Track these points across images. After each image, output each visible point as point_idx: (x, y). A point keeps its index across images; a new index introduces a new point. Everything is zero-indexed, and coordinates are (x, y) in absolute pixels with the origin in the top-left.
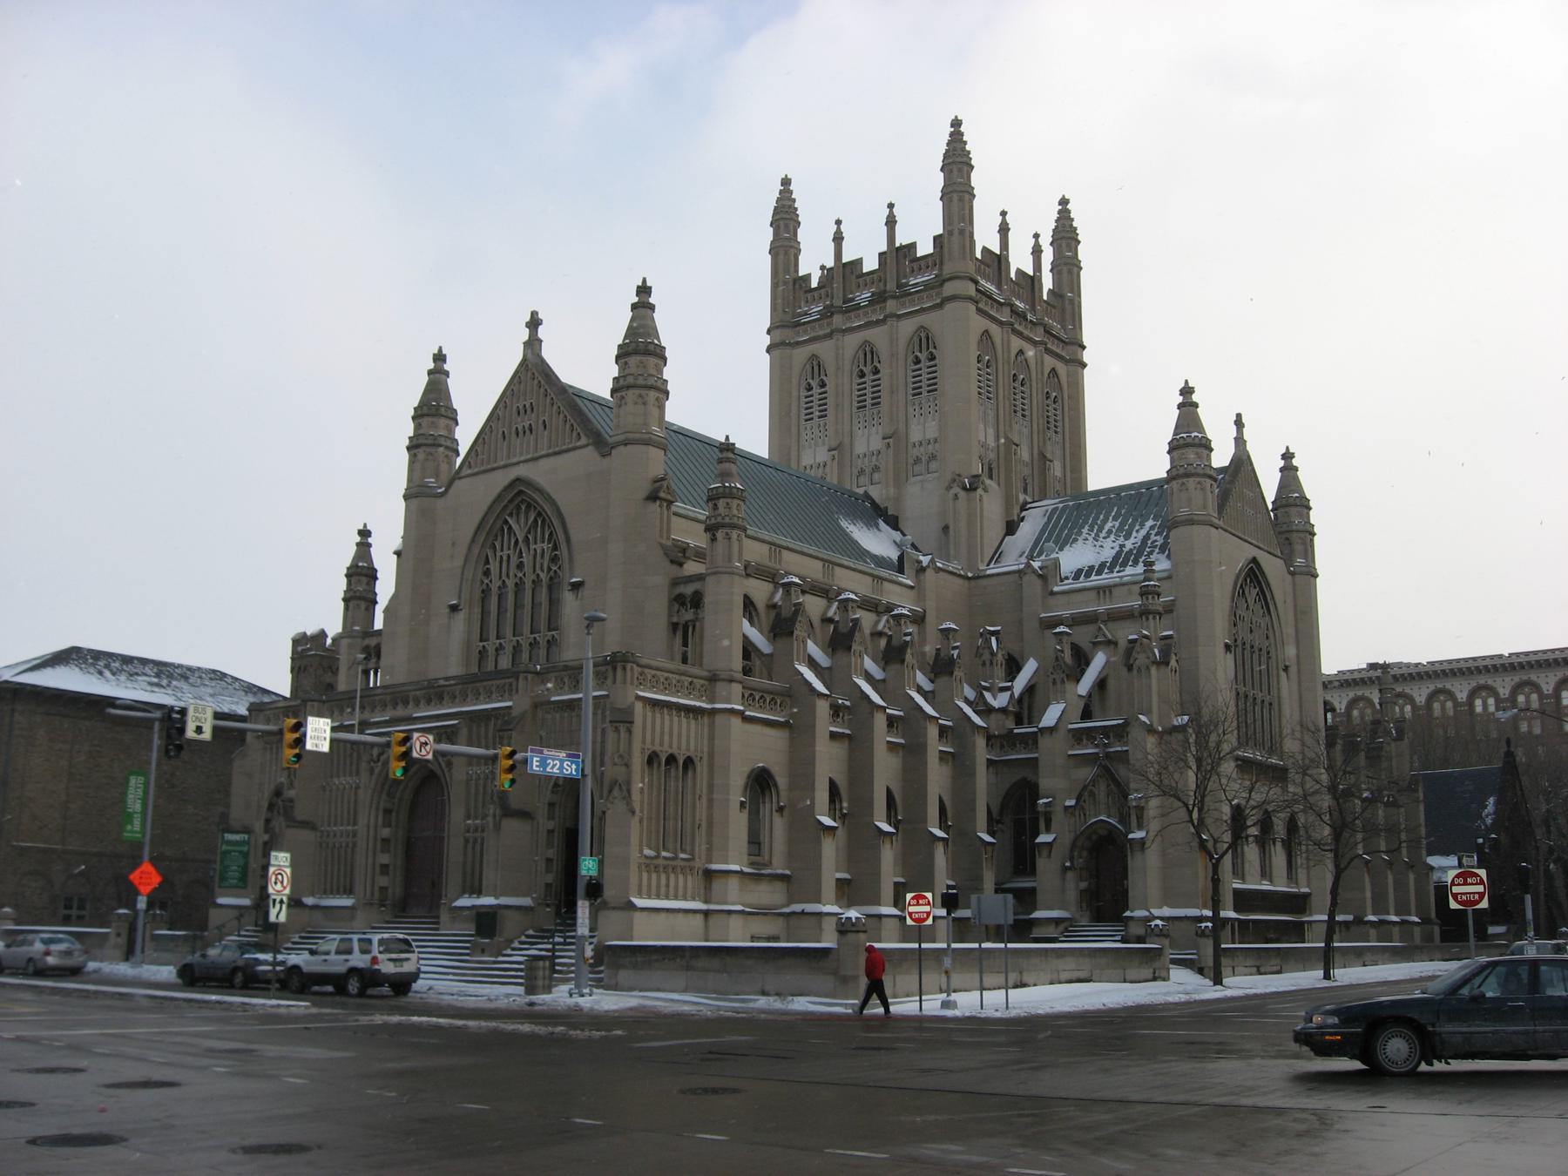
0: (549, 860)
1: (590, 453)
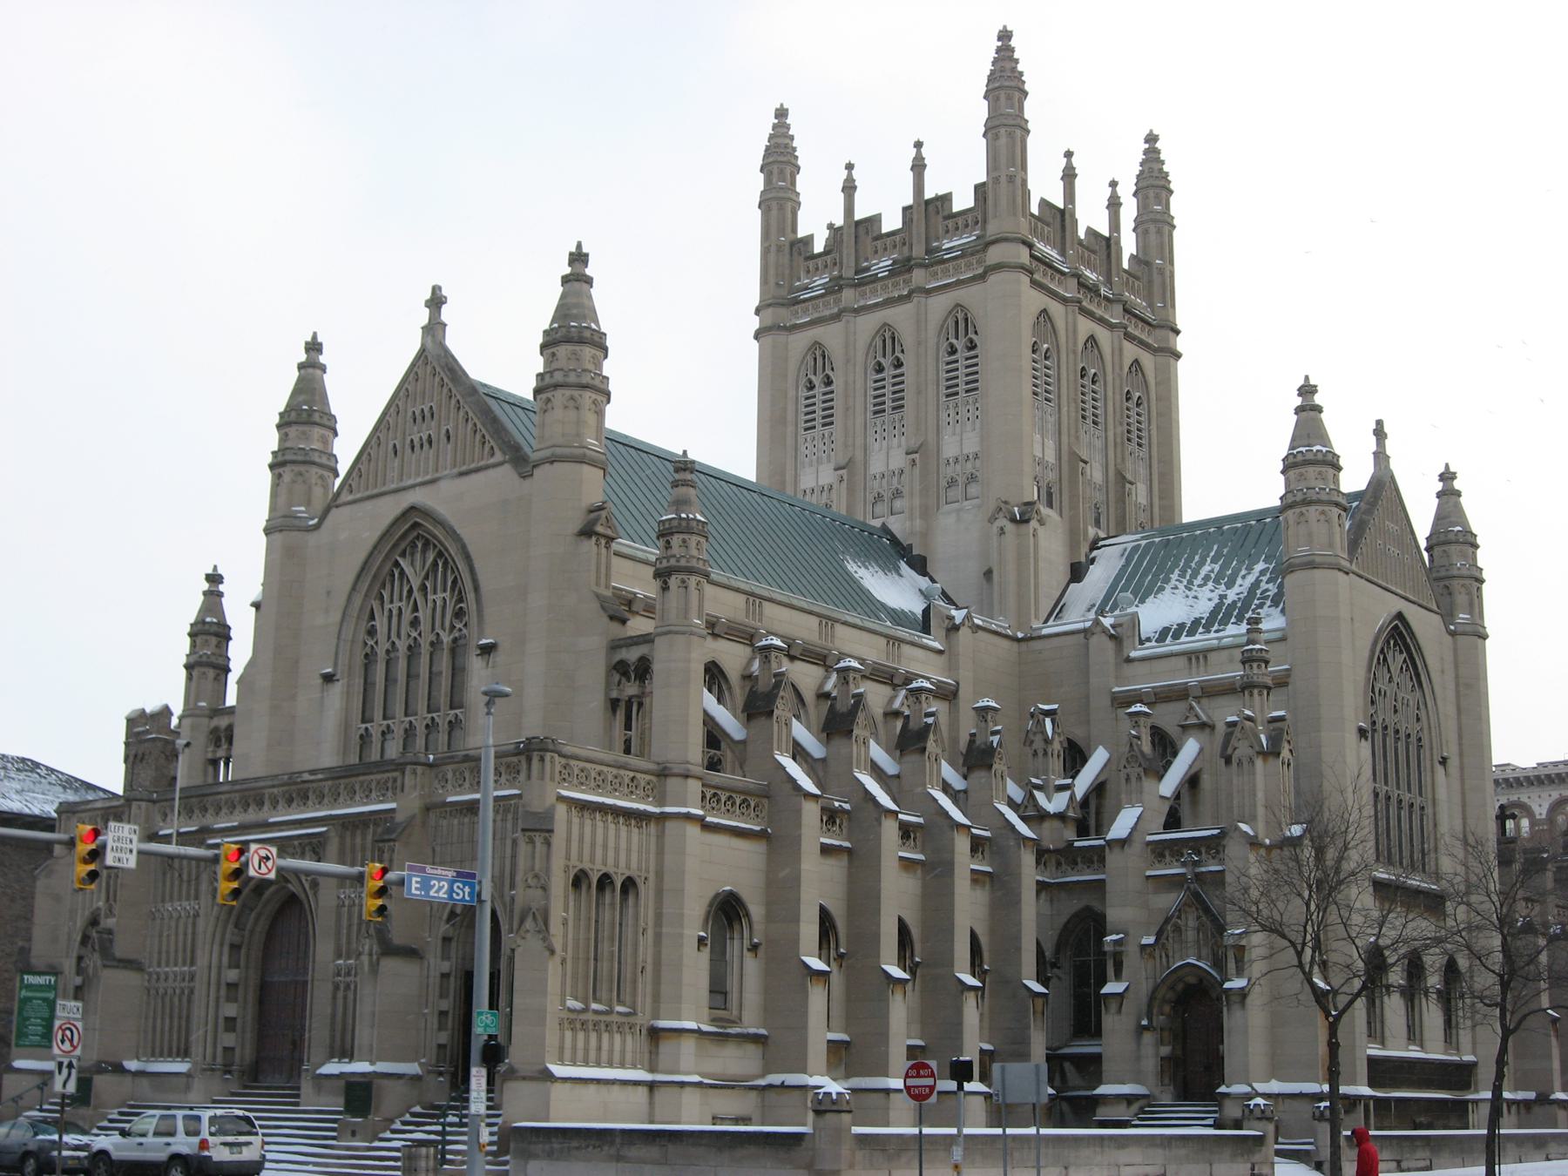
0: (443, 1014)
1: (505, 474)
